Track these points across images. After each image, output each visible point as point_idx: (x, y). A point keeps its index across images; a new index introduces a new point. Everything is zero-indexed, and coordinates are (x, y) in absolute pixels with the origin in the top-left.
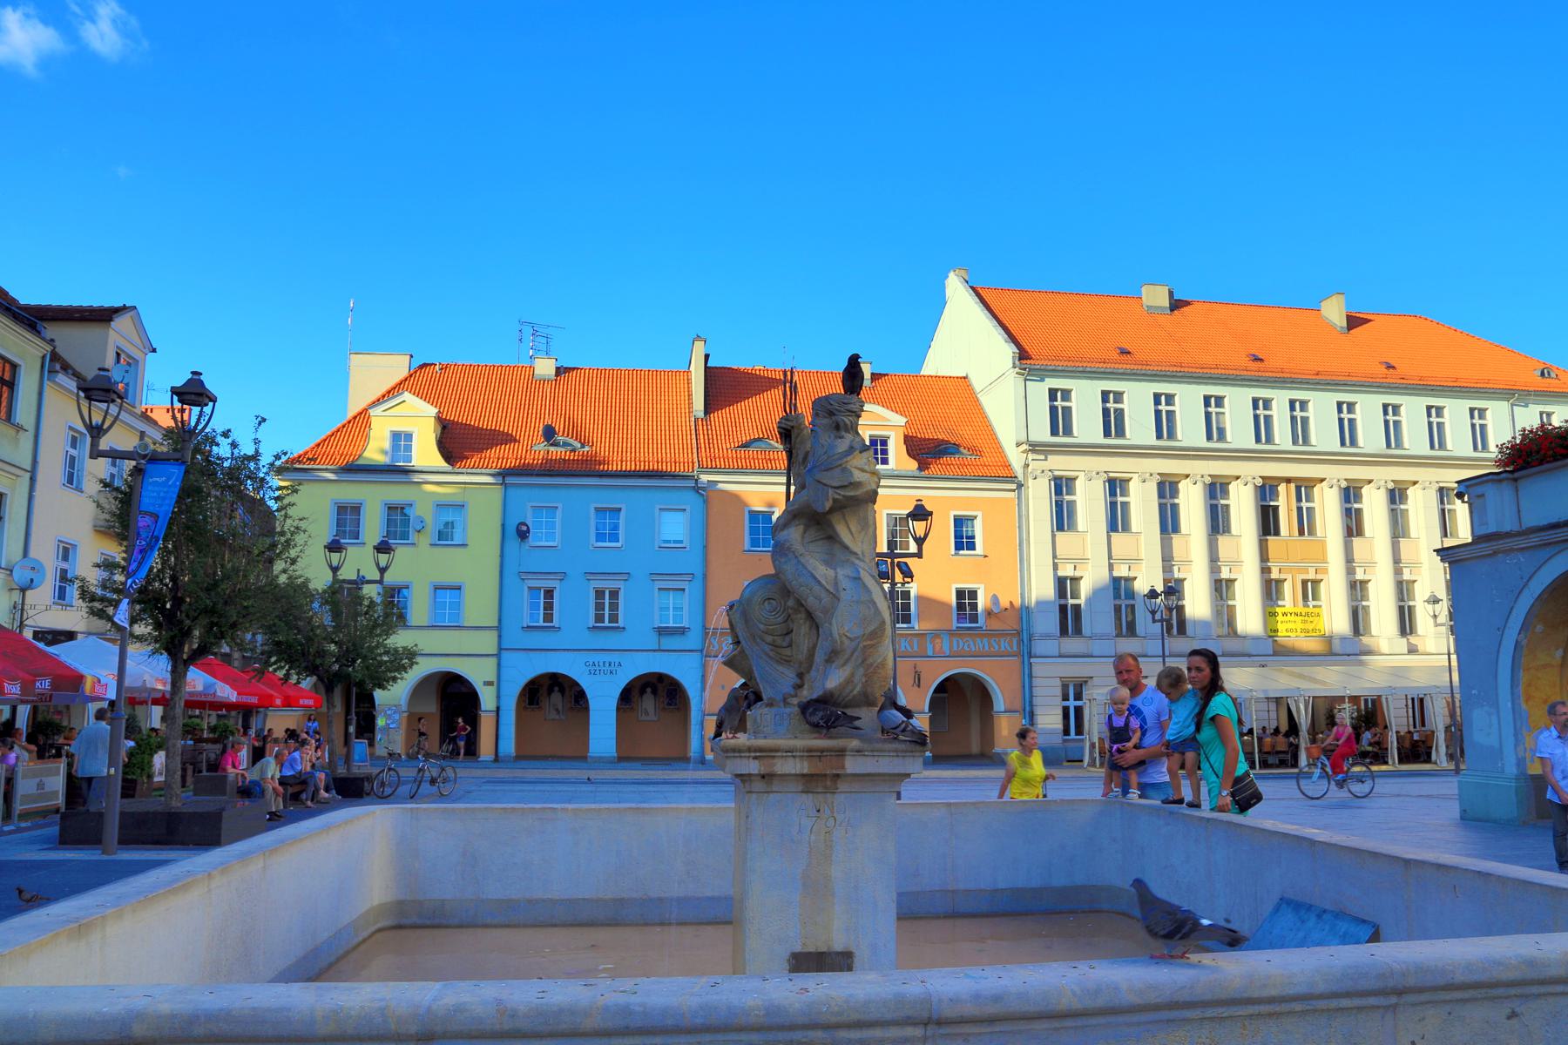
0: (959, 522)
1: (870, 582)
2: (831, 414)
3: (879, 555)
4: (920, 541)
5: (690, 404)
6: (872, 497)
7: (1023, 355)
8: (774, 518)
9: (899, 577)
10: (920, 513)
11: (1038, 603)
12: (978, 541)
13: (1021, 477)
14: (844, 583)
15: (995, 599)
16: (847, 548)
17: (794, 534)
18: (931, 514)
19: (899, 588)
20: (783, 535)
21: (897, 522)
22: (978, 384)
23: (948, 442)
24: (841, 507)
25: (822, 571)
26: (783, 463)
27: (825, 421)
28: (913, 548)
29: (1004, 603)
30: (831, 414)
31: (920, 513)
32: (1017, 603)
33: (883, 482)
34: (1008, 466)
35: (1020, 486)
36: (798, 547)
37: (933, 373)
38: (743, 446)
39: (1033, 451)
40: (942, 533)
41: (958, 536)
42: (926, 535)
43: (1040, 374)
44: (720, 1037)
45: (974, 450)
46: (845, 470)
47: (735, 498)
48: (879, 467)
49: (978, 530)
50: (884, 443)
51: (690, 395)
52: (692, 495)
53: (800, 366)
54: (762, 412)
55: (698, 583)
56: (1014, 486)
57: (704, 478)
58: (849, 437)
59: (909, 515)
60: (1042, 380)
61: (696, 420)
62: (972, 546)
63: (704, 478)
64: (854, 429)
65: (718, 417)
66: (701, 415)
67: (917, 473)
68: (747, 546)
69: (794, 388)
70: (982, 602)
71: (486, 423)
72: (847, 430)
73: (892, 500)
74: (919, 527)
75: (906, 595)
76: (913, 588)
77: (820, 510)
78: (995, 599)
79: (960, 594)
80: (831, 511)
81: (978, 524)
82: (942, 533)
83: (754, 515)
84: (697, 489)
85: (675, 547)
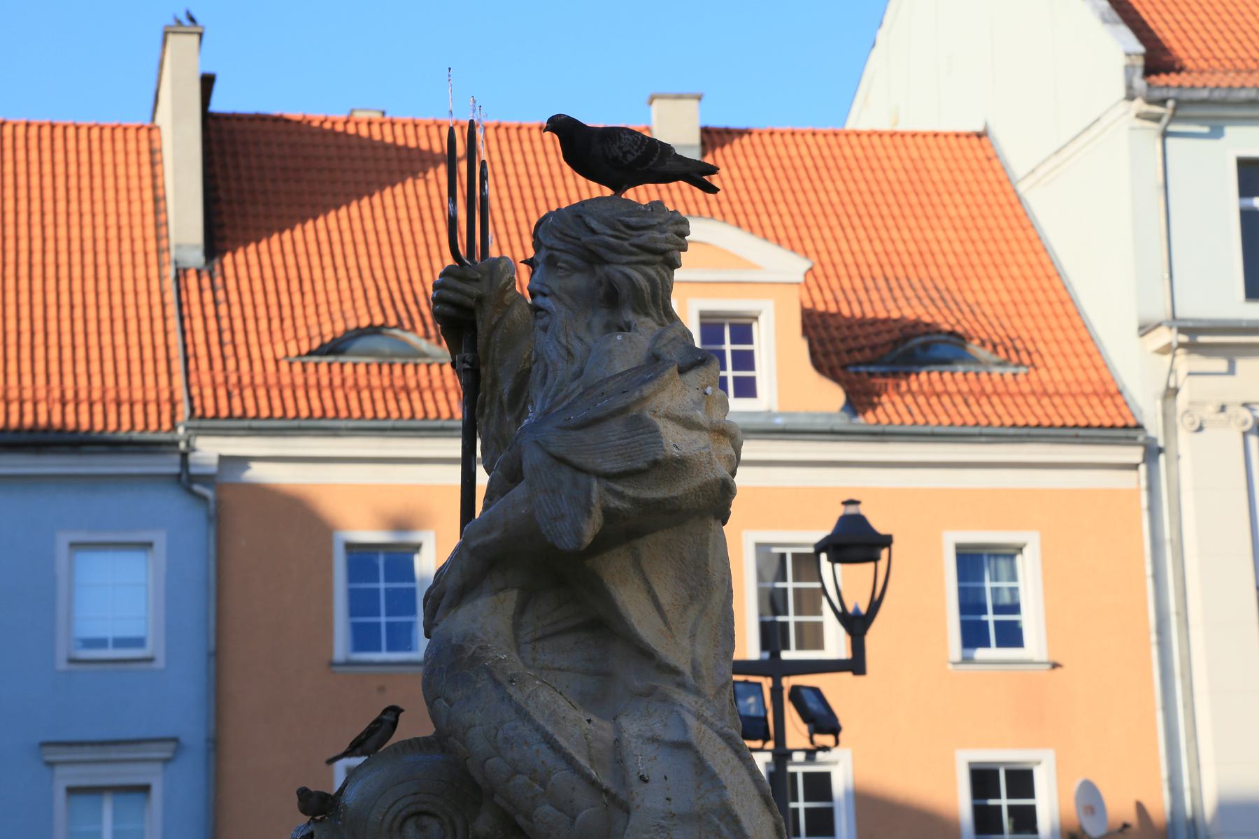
0: (971, 562)
1: (718, 757)
2: (592, 258)
3: (745, 667)
4: (856, 624)
5: (160, 226)
6: (719, 499)
7: (1157, 60)
8: (428, 563)
9: (796, 733)
10: (855, 540)
11: (1226, 809)
12: (1031, 620)
13: (1154, 427)
14: (643, 759)
15: (1090, 797)
16: (646, 654)
17: (488, 618)
18: (887, 541)
19: (798, 767)
20: (461, 621)
21: (788, 571)
22: (1018, 152)
23: (930, 329)
24: (623, 531)
25: (577, 727)
26: (448, 399)
27: (578, 281)
28: (836, 644)
29: (1119, 807)
30: (592, 258)
31: (855, 540)
32: (1160, 806)
33: (750, 449)
34: (1113, 393)
35: (1152, 452)
36: (503, 653)
37: (884, 125)
38: (334, 348)
39: (1192, 348)
40: (921, 592)
41: (970, 604)
42: (875, 606)
43: (1213, 112)
44: (1154, 638)
45: (1012, 352)
46: (642, 427)
47: (297, 516)
48: (737, 405)
49: (1030, 584)
50: (743, 332)
51: (158, 200)
52: (173, 503)
53: (488, 117)
54: (386, 250)
55: (191, 770)
56: (1134, 454)
57: (209, 450)
58: (646, 326)
59: (821, 547)
60: (1216, 133)
61: (180, 275)
62: (1011, 636)
63: (209, 450)
64: (657, 301)
65: (242, 263)
66: (196, 257)
67: (842, 422)
68: (341, 648)
69: (478, 174)
70: (1049, 805)
71: (719, 740)
72: (641, 308)
73: (775, 505)
74: (850, 582)
75: (819, 785)
76: (843, 768)
77: (567, 543)
78: (1090, 797)
79: (983, 779)
80: (602, 543)
81: (1029, 569)
82: (921, 592)
83: (361, 555)
84: (187, 479)
85: (118, 663)
